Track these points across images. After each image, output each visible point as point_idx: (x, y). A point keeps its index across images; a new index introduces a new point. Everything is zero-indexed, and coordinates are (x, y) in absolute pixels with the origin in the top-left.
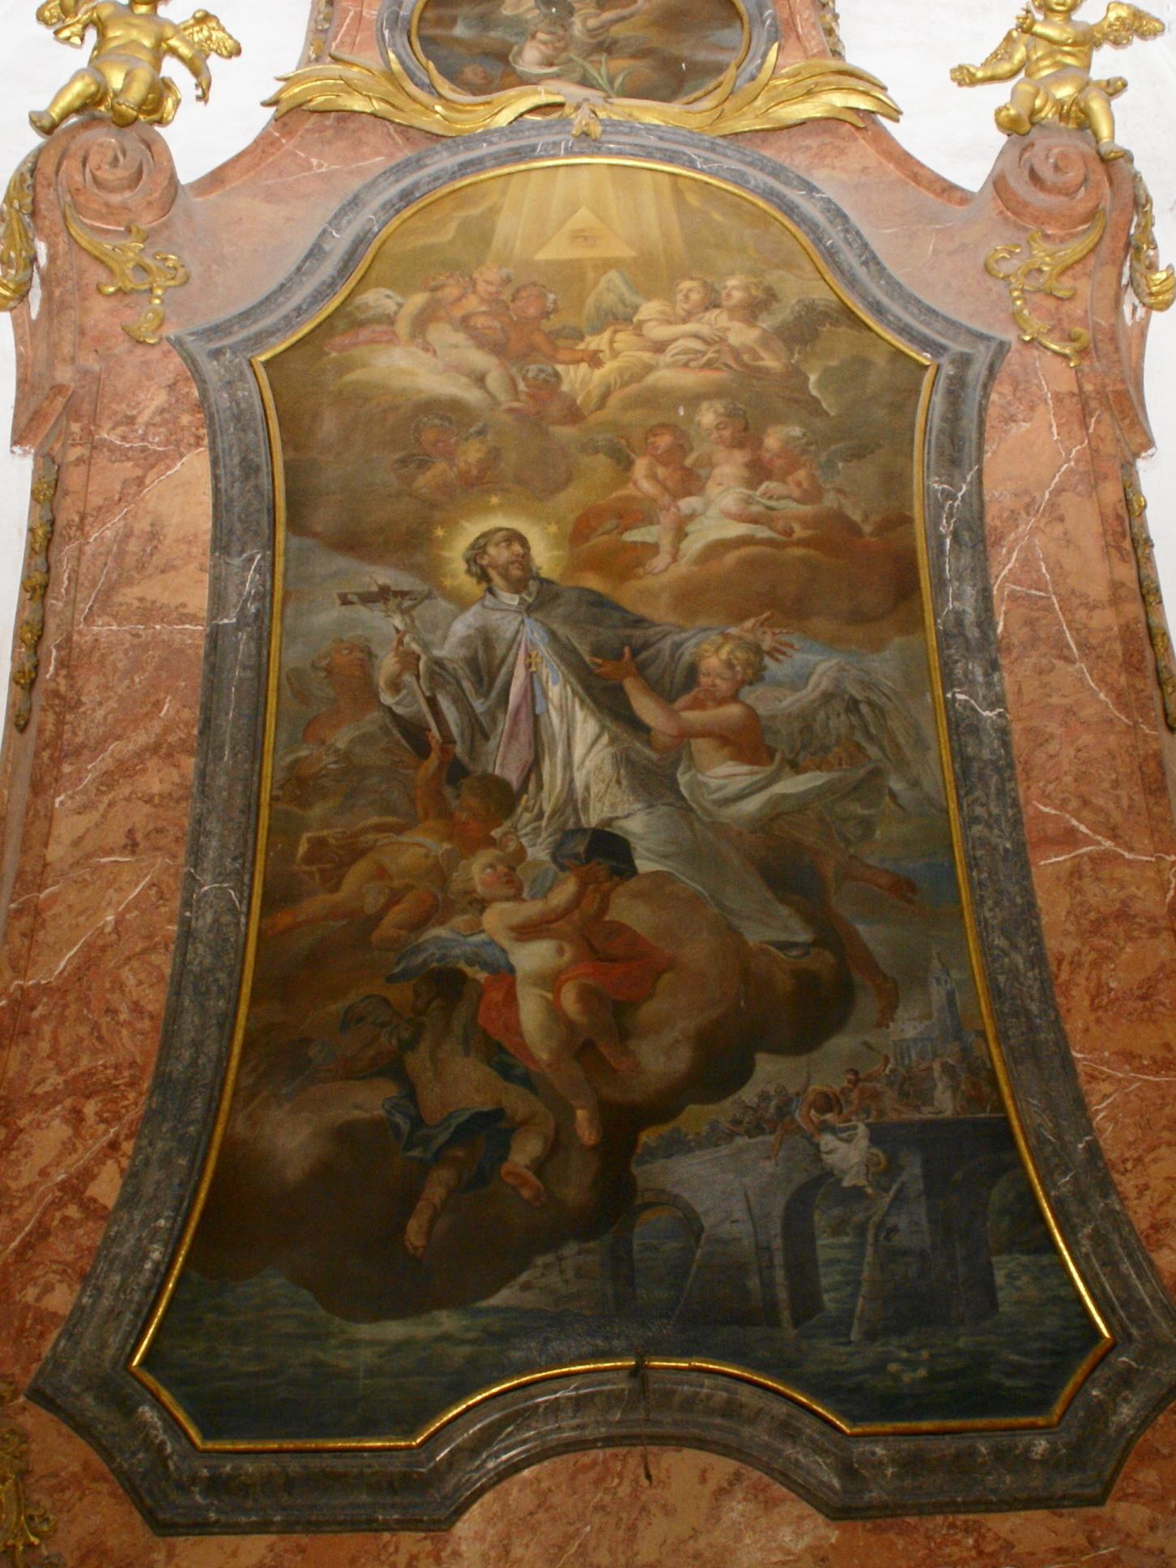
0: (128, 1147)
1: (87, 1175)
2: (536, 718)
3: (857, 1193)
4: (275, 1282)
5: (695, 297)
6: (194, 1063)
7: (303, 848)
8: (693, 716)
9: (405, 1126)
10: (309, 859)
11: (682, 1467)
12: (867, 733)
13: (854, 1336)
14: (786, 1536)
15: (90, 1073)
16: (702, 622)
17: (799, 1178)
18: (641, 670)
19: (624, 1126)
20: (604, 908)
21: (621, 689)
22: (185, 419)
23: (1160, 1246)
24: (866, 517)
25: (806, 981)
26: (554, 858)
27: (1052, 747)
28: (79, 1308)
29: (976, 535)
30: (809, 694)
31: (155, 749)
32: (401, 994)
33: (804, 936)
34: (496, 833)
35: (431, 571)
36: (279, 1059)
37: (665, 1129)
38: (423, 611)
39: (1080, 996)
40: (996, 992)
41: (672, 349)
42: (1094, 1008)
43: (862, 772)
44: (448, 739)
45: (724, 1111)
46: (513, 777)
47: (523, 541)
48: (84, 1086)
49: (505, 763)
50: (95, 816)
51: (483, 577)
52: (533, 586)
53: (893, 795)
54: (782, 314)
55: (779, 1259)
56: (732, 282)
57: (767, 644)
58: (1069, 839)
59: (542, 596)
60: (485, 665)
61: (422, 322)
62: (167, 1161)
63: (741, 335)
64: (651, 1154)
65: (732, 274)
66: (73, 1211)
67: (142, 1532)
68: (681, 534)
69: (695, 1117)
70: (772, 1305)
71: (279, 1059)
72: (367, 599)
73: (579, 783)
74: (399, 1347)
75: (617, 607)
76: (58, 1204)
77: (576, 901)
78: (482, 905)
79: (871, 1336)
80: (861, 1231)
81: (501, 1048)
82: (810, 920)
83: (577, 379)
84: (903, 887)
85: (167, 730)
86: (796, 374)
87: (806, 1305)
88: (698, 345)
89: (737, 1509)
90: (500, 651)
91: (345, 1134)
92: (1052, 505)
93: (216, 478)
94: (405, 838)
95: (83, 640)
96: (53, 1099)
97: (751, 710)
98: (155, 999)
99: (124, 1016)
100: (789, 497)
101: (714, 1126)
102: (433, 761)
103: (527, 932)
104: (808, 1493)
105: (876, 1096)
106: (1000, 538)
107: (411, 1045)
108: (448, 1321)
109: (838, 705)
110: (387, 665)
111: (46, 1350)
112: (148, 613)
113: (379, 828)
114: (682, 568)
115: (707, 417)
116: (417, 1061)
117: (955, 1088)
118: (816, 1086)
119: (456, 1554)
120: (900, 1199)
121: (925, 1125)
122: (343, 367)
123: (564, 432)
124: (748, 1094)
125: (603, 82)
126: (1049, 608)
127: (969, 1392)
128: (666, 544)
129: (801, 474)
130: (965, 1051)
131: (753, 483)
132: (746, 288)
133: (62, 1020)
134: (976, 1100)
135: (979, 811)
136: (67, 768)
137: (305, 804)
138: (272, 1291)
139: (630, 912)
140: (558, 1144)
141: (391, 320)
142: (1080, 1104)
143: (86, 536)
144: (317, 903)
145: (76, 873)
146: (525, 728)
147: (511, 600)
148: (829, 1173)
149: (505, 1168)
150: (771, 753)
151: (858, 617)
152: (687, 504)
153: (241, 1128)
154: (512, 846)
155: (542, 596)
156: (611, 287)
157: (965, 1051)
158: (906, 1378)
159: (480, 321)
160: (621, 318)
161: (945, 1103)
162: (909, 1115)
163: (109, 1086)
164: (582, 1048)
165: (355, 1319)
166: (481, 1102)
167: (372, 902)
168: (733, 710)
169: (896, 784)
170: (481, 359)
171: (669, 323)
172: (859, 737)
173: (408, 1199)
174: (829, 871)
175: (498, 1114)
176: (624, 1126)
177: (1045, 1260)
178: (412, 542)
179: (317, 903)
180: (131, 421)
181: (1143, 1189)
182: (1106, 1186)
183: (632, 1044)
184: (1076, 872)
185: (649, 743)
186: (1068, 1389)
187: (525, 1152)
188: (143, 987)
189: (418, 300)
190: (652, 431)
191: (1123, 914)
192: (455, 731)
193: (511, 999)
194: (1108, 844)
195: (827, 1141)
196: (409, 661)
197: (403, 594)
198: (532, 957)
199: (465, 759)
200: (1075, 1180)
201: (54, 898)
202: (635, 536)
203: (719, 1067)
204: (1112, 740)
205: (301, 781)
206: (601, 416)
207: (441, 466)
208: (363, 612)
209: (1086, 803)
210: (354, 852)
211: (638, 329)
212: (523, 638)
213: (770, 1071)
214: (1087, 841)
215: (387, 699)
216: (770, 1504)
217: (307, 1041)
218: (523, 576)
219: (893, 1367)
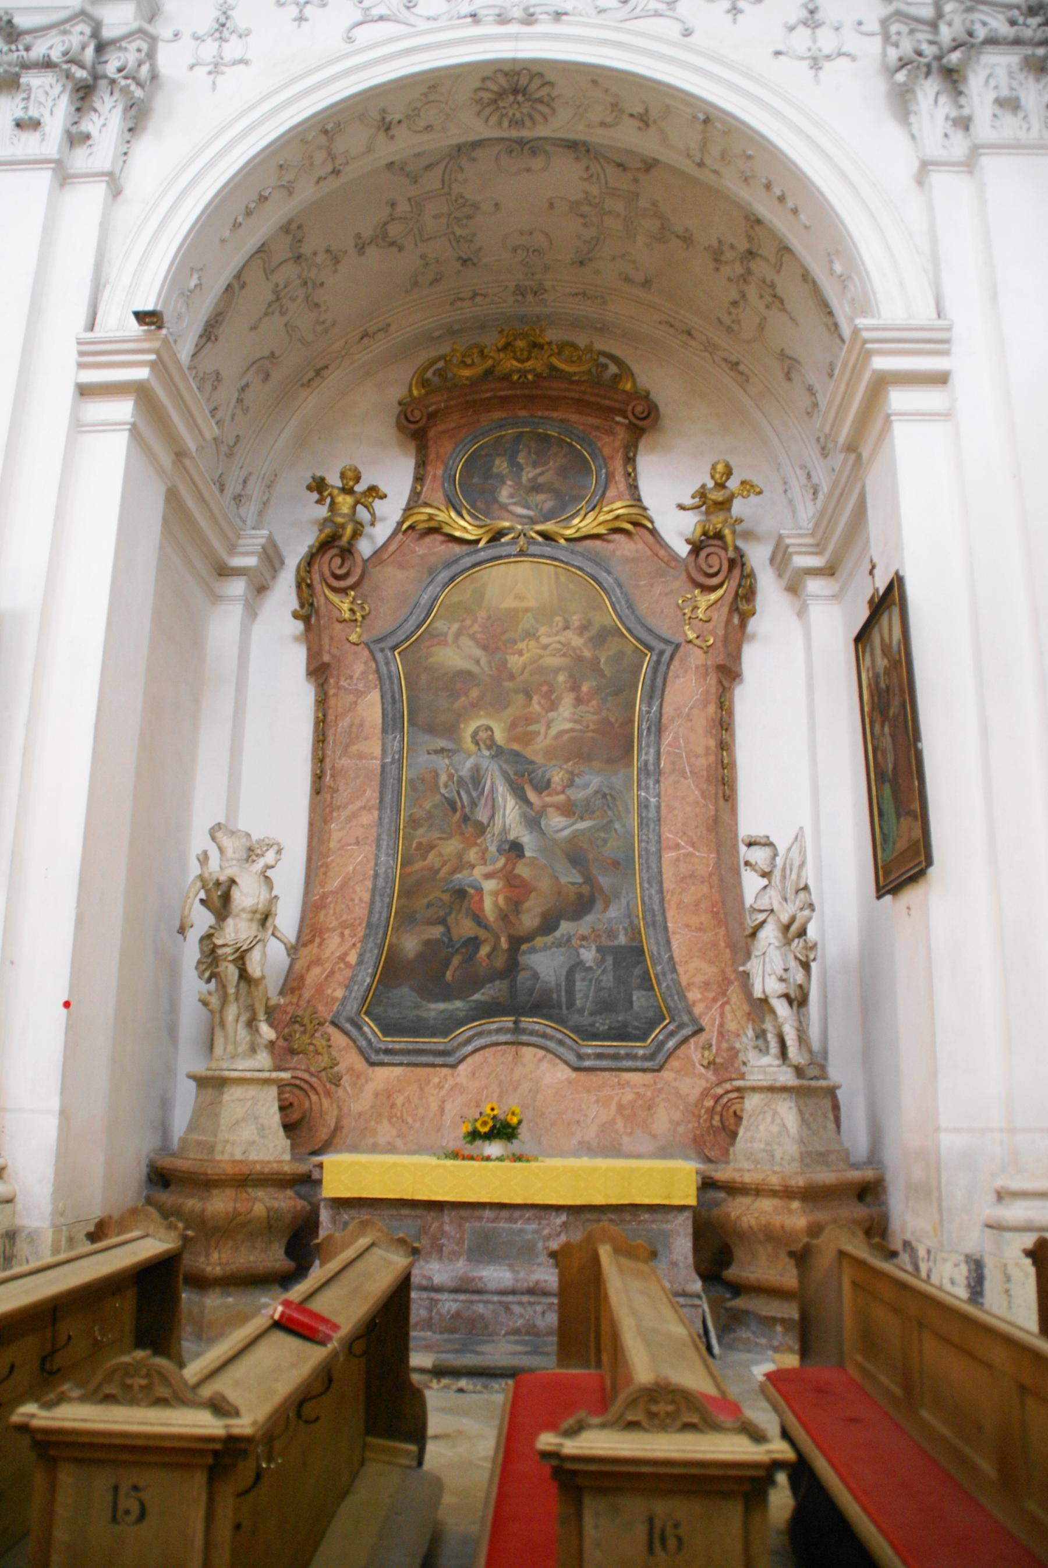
0: (359, 945)
1: (346, 954)
2: (493, 800)
3: (590, 968)
4: (405, 990)
5: (560, 624)
6: (379, 919)
7: (414, 845)
8: (548, 799)
9: (446, 940)
10: (417, 849)
11: (528, 1052)
12: (608, 806)
13: (586, 1014)
14: (559, 1075)
15: (346, 921)
16: (554, 762)
17: (572, 962)
18: (531, 781)
19: (517, 942)
20: (513, 869)
21: (523, 788)
22: (371, 677)
23: (689, 991)
24: (617, 720)
25: (580, 896)
26: (498, 851)
27: (676, 812)
28: (345, 998)
29: (658, 728)
30: (589, 791)
31: (364, 808)
32: (446, 897)
33: (580, 880)
34: (479, 841)
35: (458, 741)
36: (407, 919)
37: (529, 945)
38: (455, 758)
39: (673, 905)
40: (643, 903)
41: (550, 648)
42: (678, 908)
43: (605, 821)
44: (463, 807)
45: (549, 939)
46: (485, 821)
47: (492, 731)
48: (344, 925)
49: (482, 815)
50: (345, 832)
51: (477, 744)
52: (494, 748)
53: (615, 830)
54: (593, 631)
55: (563, 988)
56: (575, 618)
57: (576, 772)
58: (677, 847)
59: (498, 752)
60: (477, 778)
61: (458, 635)
62: (371, 950)
63: (577, 641)
64: (524, 953)
65: (575, 613)
66: (342, 965)
67: (365, 1065)
68: (548, 727)
69: (539, 941)
70: (559, 1003)
71: (407, 919)
72: (436, 752)
73: (508, 822)
74: (442, 1012)
75: (524, 757)
76: (337, 963)
77: (505, 865)
78: (473, 867)
79: (591, 1014)
80: (591, 981)
81: (478, 916)
82: (583, 875)
83: (515, 662)
84: (616, 864)
85: (368, 801)
86: (596, 660)
87: (571, 1004)
88: (559, 646)
89: (545, 1065)
90: (482, 773)
91: (427, 943)
92: (688, 715)
93: (383, 704)
94: (449, 842)
95: (338, 766)
96: (334, 929)
97: (568, 797)
98: (367, 897)
99: (356, 901)
100: (588, 712)
101: (546, 944)
102: (458, 815)
103: (488, 876)
104: (566, 1062)
105: (599, 936)
106: (667, 728)
107: (449, 914)
108: (458, 1004)
109: (599, 796)
110: (443, 778)
111: (335, 1008)
112: (360, 756)
113: (440, 839)
114: (548, 741)
115: (561, 678)
116: (451, 920)
117: (626, 934)
118: (580, 932)
119: (458, 1075)
120: (604, 971)
121: (615, 947)
122: (427, 657)
123: (507, 684)
124: (557, 934)
125: (533, 507)
126: (682, 757)
127: (621, 1034)
128: (543, 730)
129: (594, 703)
130: (631, 922)
131: (575, 706)
132: (580, 620)
133: (336, 902)
134: (633, 939)
135: (644, 837)
136: (335, 814)
137: (415, 830)
138: (405, 993)
139: (522, 870)
140: (494, 949)
141: (446, 635)
142: (668, 942)
143: (337, 725)
144: (418, 865)
145: (340, 852)
146: (490, 803)
147: (486, 753)
148: (581, 962)
149: (478, 956)
150: (574, 814)
151: (610, 761)
152: (552, 715)
153: (394, 940)
154: (484, 846)
155: (498, 752)
156: (527, 622)
157: (631, 922)
158: (601, 1029)
159: (479, 636)
160: (531, 635)
161: (622, 940)
162: (611, 944)
163: (352, 925)
164: (504, 917)
165: (429, 1001)
166: (471, 934)
167: (437, 866)
168: (562, 797)
169: (617, 826)
170: (478, 652)
171: (549, 636)
172: (605, 808)
173: (447, 963)
174: (590, 856)
175: (476, 938)
176: (517, 942)
177: (650, 993)
178: (451, 730)
179: (418, 865)
180: (351, 677)
181: (686, 972)
182: (674, 970)
183: (520, 916)
184: (678, 860)
185: (532, 809)
186: (653, 1036)
187: (484, 950)
188: (363, 892)
189: (456, 626)
190: (541, 685)
191: (692, 876)
192: (466, 803)
193: (481, 900)
194: (691, 849)
195: (582, 951)
196: (451, 776)
197: (449, 750)
198: (490, 886)
199: (469, 814)
200: (663, 968)
201: (332, 861)
202: (531, 728)
203: (548, 925)
204: (697, 810)
205: (414, 821)
206: (521, 678)
207: (463, 698)
208: (434, 757)
209: (685, 833)
210: (431, 847)
211: (537, 639)
212: (490, 768)
213: (565, 927)
214: (683, 848)
215: (443, 791)
216: (555, 1065)
217: (415, 912)
218: (491, 744)
219: (597, 1025)
